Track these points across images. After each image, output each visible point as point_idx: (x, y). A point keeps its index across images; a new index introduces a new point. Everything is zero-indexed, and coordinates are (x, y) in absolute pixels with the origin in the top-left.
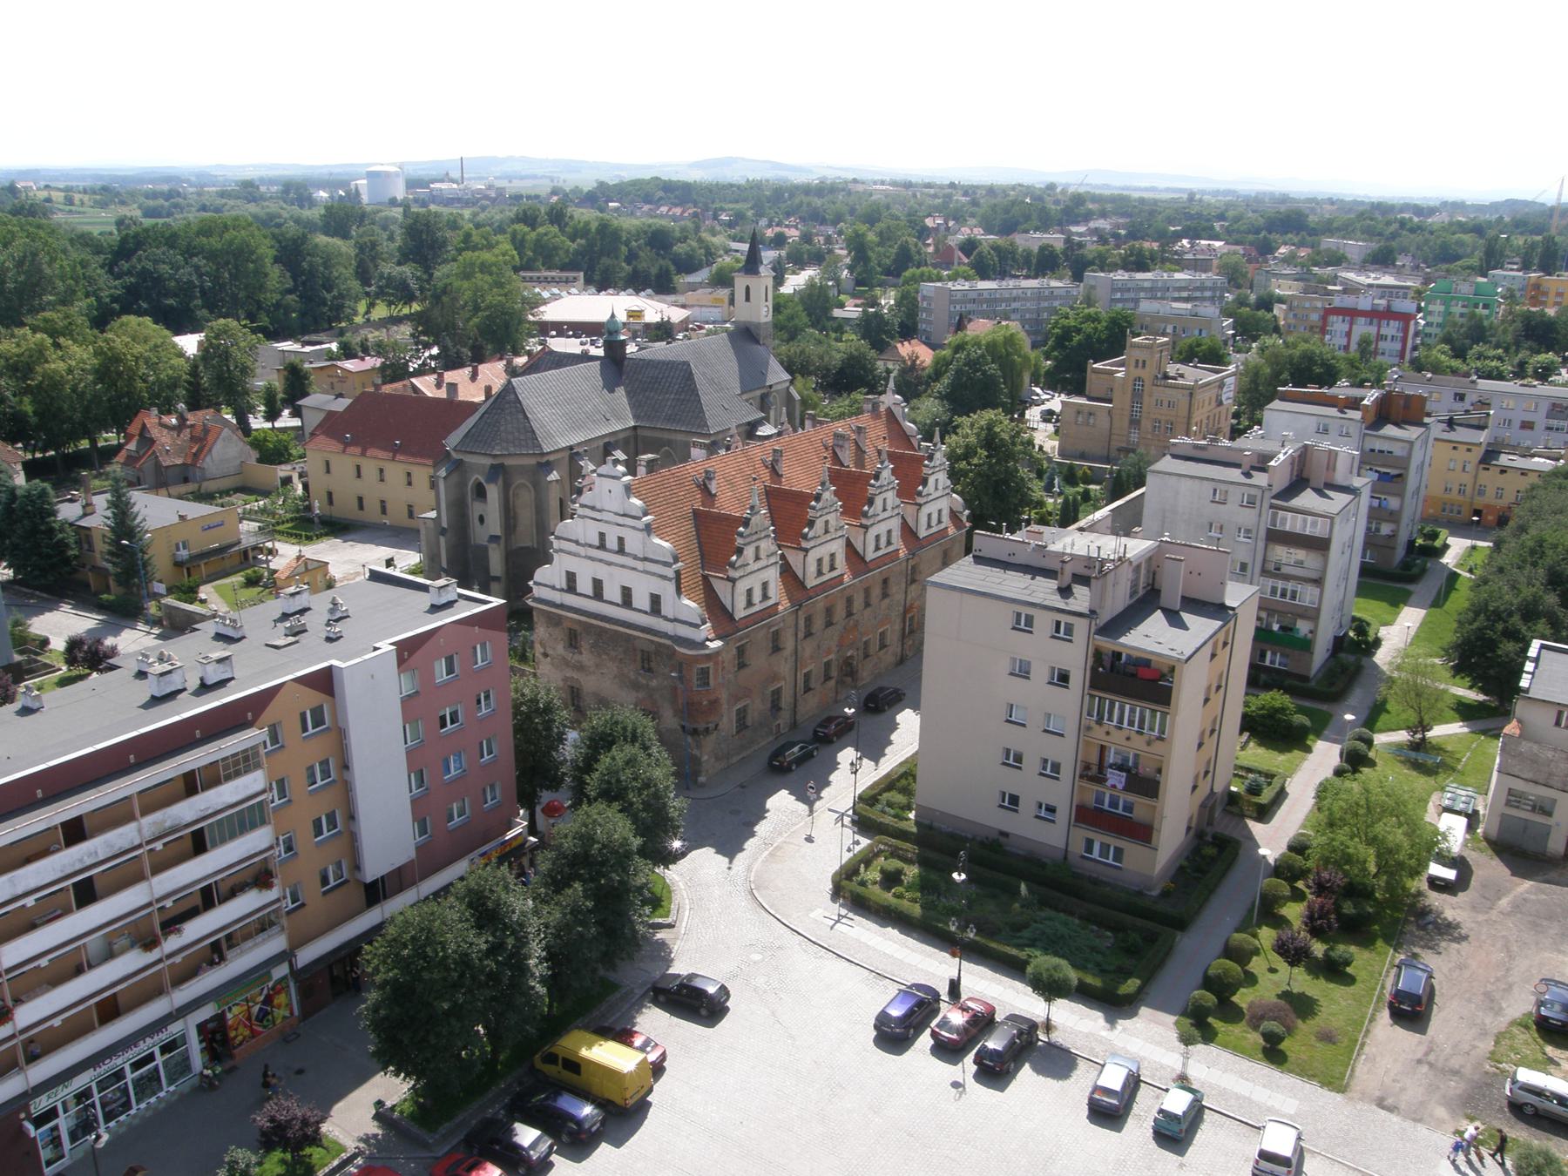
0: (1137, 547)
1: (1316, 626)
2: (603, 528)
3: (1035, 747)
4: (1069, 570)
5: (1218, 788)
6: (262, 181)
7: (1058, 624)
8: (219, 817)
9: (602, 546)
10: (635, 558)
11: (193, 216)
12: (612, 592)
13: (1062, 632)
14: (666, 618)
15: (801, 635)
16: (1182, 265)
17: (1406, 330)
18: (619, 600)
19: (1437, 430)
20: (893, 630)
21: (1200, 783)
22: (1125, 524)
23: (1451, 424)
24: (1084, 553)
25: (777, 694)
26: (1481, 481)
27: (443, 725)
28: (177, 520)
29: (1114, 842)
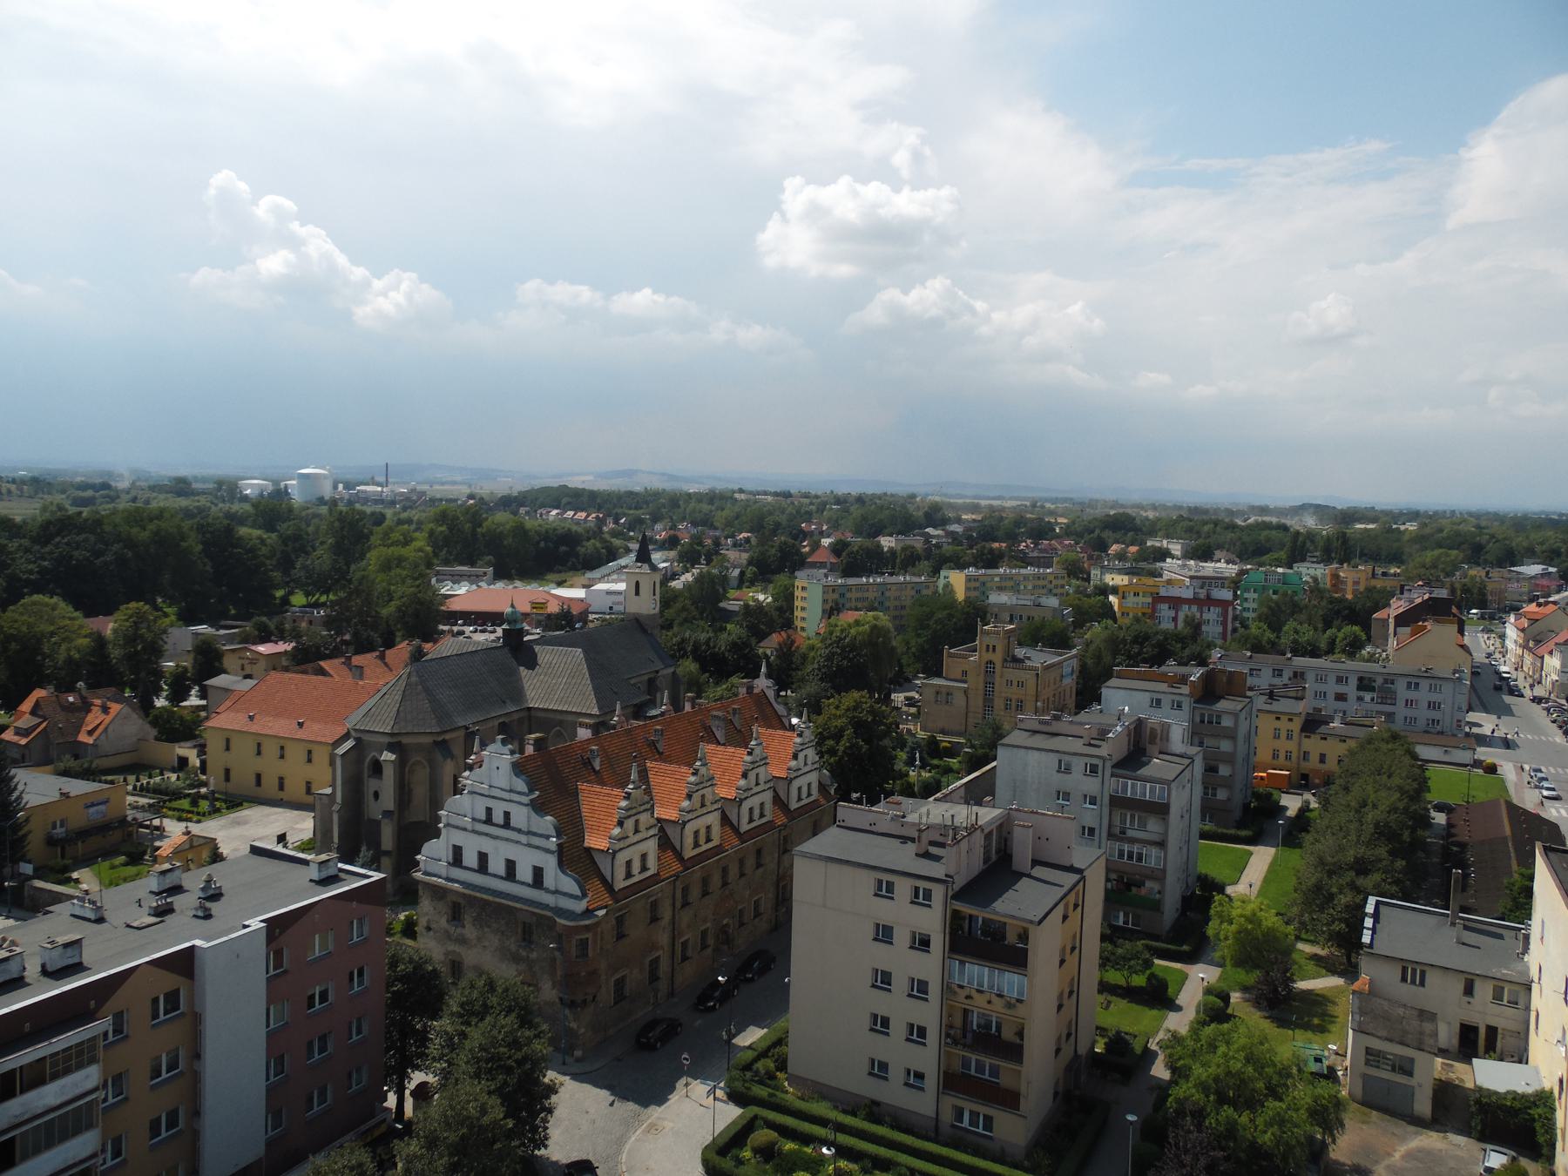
0: (987, 815)
3: (900, 1008)
4: (926, 837)
5: (1082, 1050)
6: (196, 479)
8: (24, 1128)
9: (489, 821)
10: (519, 831)
11: (123, 504)
12: (497, 866)
13: (921, 898)
14: (547, 891)
15: (678, 905)
16: (1025, 561)
19: (1260, 702)
21: (1063, 1046)
22: (977, 794)
23: (1271, 696)
24: (938, 820)
25: (655, 963)
26: (1305, 748)
27: (311, 1004)
29: (983, 1110)
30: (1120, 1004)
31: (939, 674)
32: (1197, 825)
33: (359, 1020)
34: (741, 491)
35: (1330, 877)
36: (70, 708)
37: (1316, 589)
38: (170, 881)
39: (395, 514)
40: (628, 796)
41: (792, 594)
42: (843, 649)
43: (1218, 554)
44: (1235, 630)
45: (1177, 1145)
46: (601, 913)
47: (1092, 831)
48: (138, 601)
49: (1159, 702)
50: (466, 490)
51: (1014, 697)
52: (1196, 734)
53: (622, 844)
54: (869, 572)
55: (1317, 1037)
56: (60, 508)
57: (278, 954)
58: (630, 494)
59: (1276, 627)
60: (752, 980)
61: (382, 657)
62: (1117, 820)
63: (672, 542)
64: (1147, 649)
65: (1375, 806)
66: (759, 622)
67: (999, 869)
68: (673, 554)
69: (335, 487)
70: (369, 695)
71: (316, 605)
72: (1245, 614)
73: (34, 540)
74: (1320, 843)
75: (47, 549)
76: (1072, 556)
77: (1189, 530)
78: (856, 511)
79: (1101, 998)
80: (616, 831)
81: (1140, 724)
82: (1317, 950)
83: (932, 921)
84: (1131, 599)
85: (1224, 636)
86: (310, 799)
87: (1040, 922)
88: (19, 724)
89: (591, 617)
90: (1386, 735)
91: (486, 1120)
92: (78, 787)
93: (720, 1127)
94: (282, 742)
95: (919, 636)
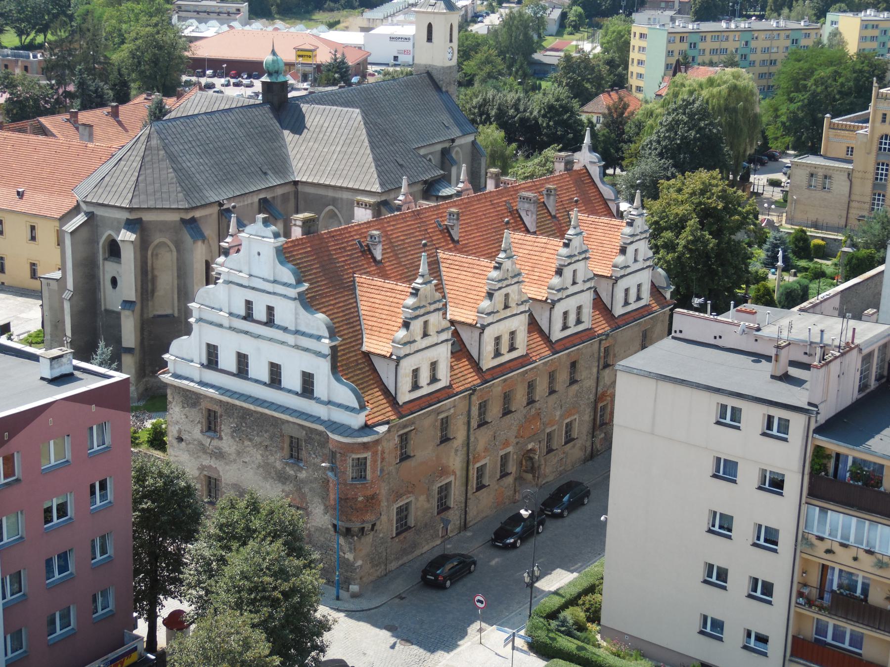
2: (251, 295)
3: (742, 559)
4: (786, 356)
7: (770, 419)
9: (248, 316)
10: (285, 329)
12: (259, 369)
13: (774, 429)
14: (318, 401)
15: (474, 423)
18: (266, 378)
20: (582, 422)
22: (855, 306)
24: (804, 336)
25: (444, 491)
31: (815, 150)
33: (103, 538)
40: (415, 293)
41: (627, 44)
42: (691, 116)
60: (560, 516)
61: (115, 114)
66: (584, 80)
71: (31, 47)
80: (402, 334)
83: (789, 458)
86: (35, 284)
91: (249, 655)
95: (791, 100)
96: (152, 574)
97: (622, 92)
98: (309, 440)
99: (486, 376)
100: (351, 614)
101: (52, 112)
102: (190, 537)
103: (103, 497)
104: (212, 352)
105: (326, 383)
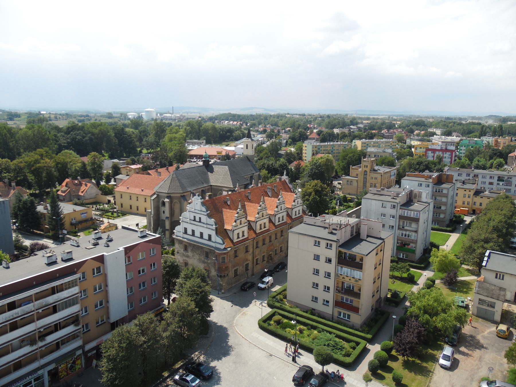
1: (416, 245)
2: (195, 215)
3: (322, 281)
4: (331, 227)
5: (383, 296)
6: (115, 113)
7: (328, 244)
9: (194, 220)
10: (204, 223)
11: (92, 121)
13: (328, 246)
14: (213, 242)
15: (255, 247)
16: (383, 136)
17: (452, 155)
19: (459, 185)
23: (464, 183)
24: (336, 222)
25: (247, 265)
26: (474, 201)
28: (72, 211)
29: (347, 313)
30: (398, 282)
31: (349, 175)
32: (430, 226)
33: (154, 278)
34: (288, 114)
35: (475, 244)
36: (76, 185)
37: (488, 146)
38: (98, 236)
39: (175, 123)
40: (238, 213)
41: (302, 149)
42: (317, 166)
43: (454, 134)
44: (455, 160)
45: (408, 326)
46: (229, 249)
47: (393, 226)
48: (94, 152)
49: (421, 184)
50: (198, 115)
51: (373, 183)
52: (435, 195)
53: (236, 228)
54: (330, 141)
55: (464, 295)
56: (74, 123)
57: (129, 257)
58: (251, 115)
59: (471, 159)
60: (278, 271)
61: (167, 169)
62: (401, 224)
63: (264, 131)
64: (421, 167)
65: (494, 220)
66: (290, 158)
67: (356, 238)
68: (264, 135)
69: (157, 115)
70: (161, 181)
71: (150, 153)
72: (461, 155)
73: (66, 133)
74: (473, 233)
75: (69, 136)
76: (400, 135)
77: (444, 125)
78: (327, 120)
79: (391, 280)
80: (234, 224)
81: (411, 192)
82: (468, 267)
83: (332, 254)
84: (419, 150)
85: (451, 162)
86: (145, 213)
87: (367, 255)
88: (62, 189)
89: (236, 156)
90: (503, 197)
91: (189, 308)
92: (78, 208)
93: (263, 315)
94: (130, 195)
95: (343, 162)
96: (168, 288)
97: (300, 161)
98: (210, 252)
99: (257, 235)
100: (222, 298)
101: (150, 169)
102: (178, 278)
103: (154, 267)
104: (186, 229)
105: (214, 237)
